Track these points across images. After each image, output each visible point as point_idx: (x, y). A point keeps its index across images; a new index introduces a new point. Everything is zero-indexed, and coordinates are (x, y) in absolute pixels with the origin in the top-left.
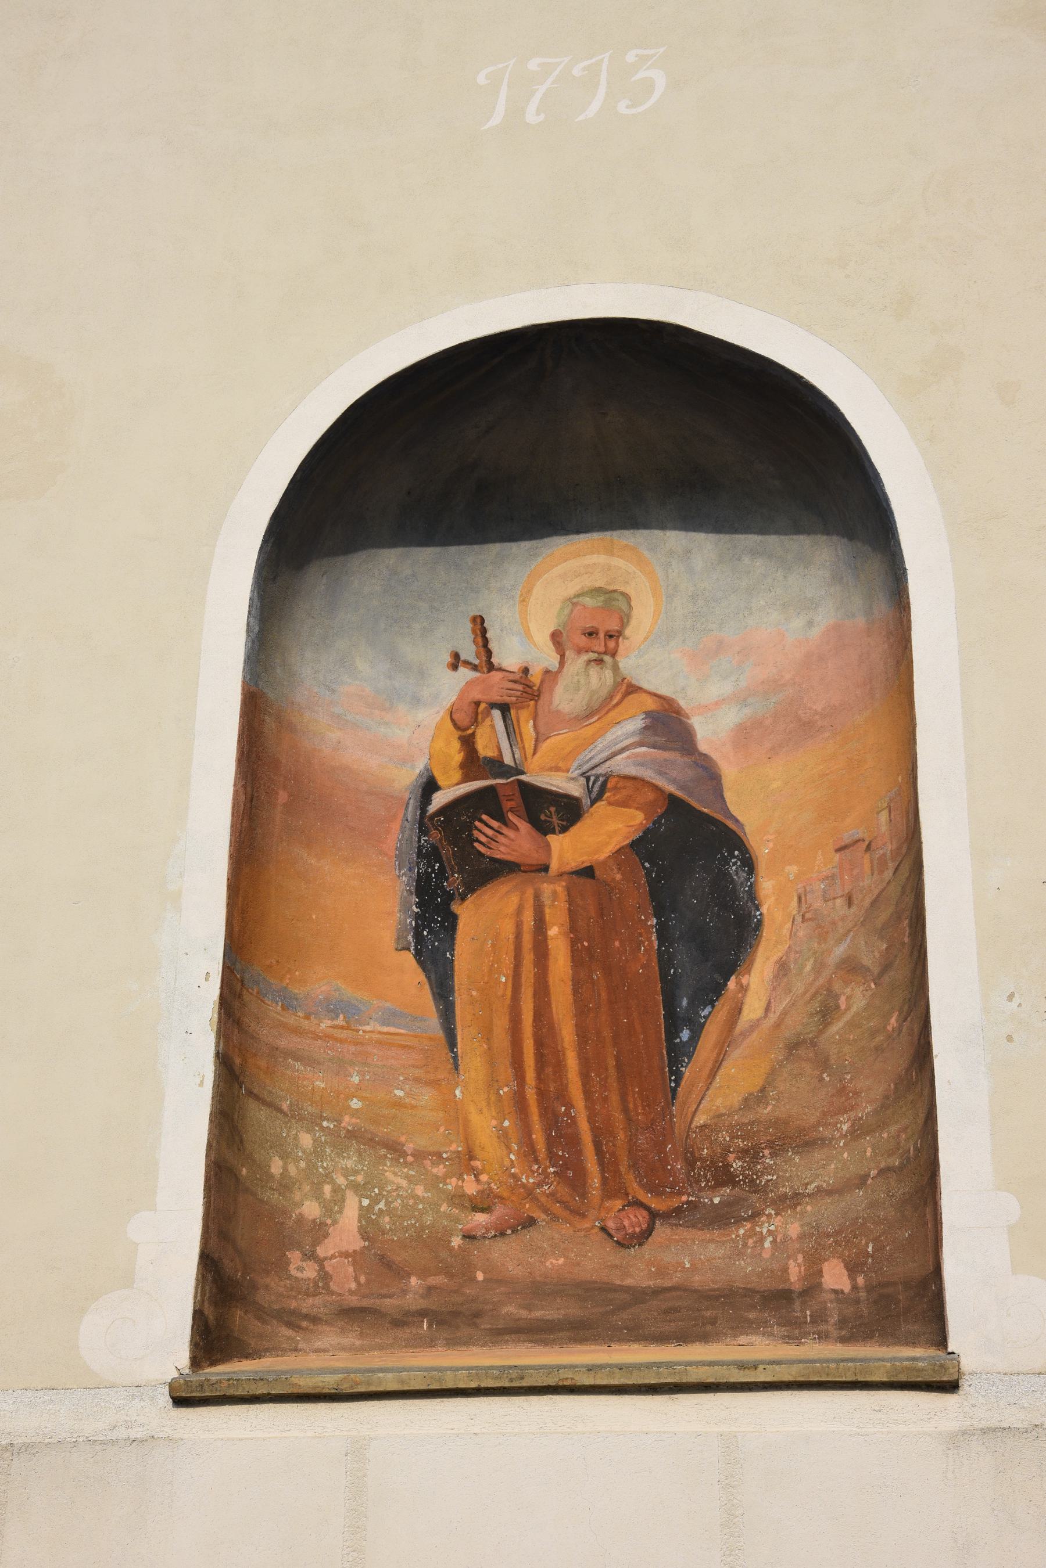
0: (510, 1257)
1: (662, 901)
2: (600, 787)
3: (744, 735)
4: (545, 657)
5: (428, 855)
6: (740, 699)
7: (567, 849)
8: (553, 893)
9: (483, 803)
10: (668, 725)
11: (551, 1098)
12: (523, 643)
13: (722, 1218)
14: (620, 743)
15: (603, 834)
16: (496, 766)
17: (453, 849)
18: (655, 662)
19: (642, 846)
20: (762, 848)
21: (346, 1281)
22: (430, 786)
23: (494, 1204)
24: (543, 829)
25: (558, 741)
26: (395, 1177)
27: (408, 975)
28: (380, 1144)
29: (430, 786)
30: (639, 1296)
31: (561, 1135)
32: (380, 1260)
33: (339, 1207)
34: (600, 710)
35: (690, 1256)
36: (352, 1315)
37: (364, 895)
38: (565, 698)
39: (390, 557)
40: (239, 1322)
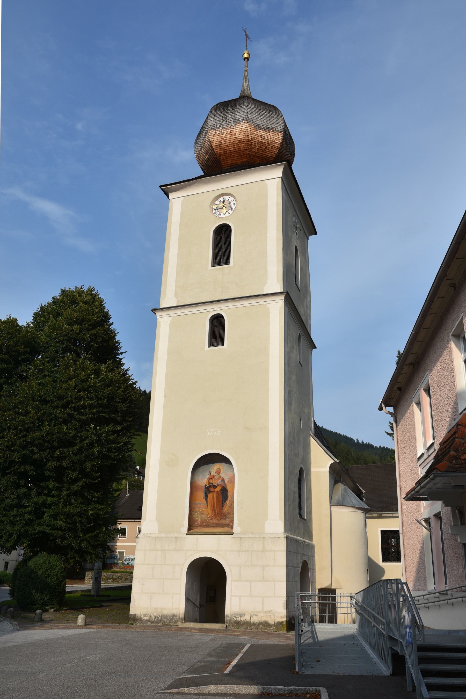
0: (211, 521)
1: (222, 494)
2: (218, 485)
3: (228, 481)
4: (215, 474)
5: (206, 491)
6: (228, 479)
7: (216, 490)
8: (215, 493)
9: (210, 486)
10: (223, 480)
11: (214, 509)
12: (213, 473)
13: (225, 519)
14: (220, 481)
15: (219, 489)
16: (211, 483)
17: (208, 490)
18: (222, 475)
19: (221, 490)
20: (229, 491)
21: (200, 524)
22: (206, 485)
23: (67, 561)
24: (214, 488)
25: (216, 481)
26: (203, 516)
27: (204, 500)
28: (202, 513)
29: (206, 485)
30: (220, 524)
31: (215, 512)
32: (202, 522)
33: (199, 518)
34: (219, 478)
35: (223, 521)
36: (200, 526)
37: (201, 495)
38: (216, 478)
39: (203, 467)
40: (191, 527)
